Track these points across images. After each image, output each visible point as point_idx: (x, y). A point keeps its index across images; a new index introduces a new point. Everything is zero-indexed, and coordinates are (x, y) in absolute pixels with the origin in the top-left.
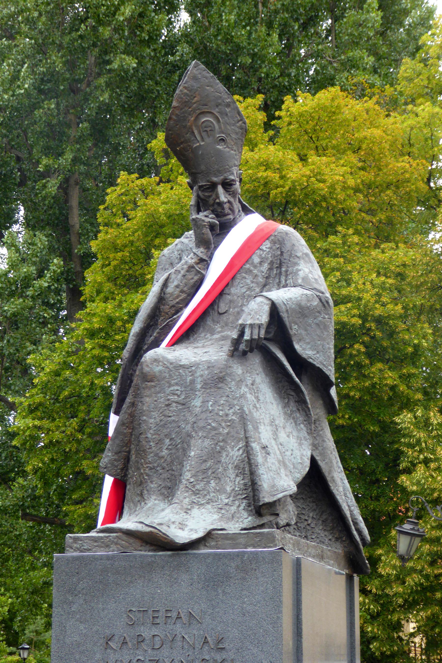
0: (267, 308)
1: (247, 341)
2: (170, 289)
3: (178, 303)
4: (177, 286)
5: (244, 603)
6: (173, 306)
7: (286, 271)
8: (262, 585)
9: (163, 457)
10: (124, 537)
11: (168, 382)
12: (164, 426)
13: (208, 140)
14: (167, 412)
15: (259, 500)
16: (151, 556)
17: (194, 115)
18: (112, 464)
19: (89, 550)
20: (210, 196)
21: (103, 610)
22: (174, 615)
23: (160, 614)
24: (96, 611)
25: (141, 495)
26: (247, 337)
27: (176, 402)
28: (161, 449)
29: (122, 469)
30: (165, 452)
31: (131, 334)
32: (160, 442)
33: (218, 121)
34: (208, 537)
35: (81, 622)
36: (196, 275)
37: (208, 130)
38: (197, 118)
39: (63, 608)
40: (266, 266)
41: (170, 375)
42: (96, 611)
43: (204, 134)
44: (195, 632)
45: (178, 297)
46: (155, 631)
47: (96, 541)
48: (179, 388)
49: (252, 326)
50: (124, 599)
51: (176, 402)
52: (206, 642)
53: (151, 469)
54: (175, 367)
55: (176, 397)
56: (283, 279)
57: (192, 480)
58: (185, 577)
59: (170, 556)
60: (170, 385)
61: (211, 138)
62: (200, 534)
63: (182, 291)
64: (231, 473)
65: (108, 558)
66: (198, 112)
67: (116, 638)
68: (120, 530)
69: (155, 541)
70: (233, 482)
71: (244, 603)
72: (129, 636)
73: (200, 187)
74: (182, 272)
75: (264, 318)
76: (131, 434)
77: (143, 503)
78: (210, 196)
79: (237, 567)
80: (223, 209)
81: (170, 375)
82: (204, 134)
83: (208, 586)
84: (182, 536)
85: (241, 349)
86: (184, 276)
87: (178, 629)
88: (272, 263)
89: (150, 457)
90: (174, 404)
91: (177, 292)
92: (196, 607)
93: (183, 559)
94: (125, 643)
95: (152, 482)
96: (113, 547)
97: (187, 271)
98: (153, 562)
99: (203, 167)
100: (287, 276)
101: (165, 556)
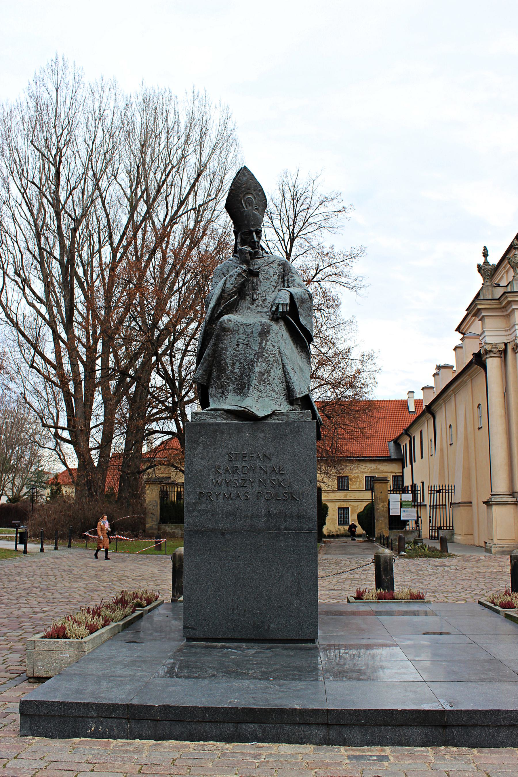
0: (288, 296)
1: (280, 312)
2: (228, 285)
3: (232, 293)
4: (232, 284)
5: (295, 449)
6: (230, 294)
7: (288, 280)
8: (305, 440)
9: (236, 373)
10: (225, 414)
11: (238, 333)
12: (236, 356)
13: (250, 208)
14: (237, 349)
15: (293, 396)
16: (242, 424)
17: (243, 194)
18: (202, 377)
19: (204, 420)
20: (248, 238)
21: (214, 452)
22: (255, 455)
23: (247, 455)
24: (210, 453)
25: (223, 393)
26: (281, 310)
27: (243, 344)
28: (234, 369)
29: (207, 380)
30: (237, 370)
31: (209, 307)
32: (233, 365)
33: (255, 198)
34: (273, 413)
35: (201, 459)
36: (242, 278)
37: (249, 203)
38: (244, 196)
39: (191, 451)
40: (276, 277)
41: (238, 329)
42: (210, 453)
43: (247, 204)
44: (267, 465)
45: (232, 289)
46: (244, 464)
47: (209, 415)
48: (244, 336)
49: (283, 304)
50: (227, 447)
51: (243, 344)
52: (274, 470)
53: (228, 379)
54: (241, 325)
55: (242, 340)
56: (286, 284)
57: (257, 384)
58: (262, 435)
59: (252, 424)
60: (239, 334)
61: (251, 207)
62: (270, 413)
63: (234, 287)
64: (277, 381)
65: (217, 424)
66: (245, 192)
67: (222, 467)
68: (223, 410)
69: (245, 416)
70: (279, 387)
71: (295, 449)
72: (230, 467)
73: (243, 233)
74: (234, 277)
75: (288, 301)
76: (213, 361)
77: (224, 398)
78: (248, 238)
79: (291, 430)
80: (255, 245)
81: (238, 329)
82: (247, 204)
83: (274, 440)
84: (261, 414)
85: (276, 316)
86: (235, 279)
87: (258, 463)
88: (279, 276)
89: (228, 372)
90: (241, 344)
91: (232, 287)
92: (267, 452)
93: (260, 425)
94: (227, 470)
95: (229, 386)
96: (219, 418)
97: (238, 276)
98: (242, 427)
99: (246, 222)
100: (288, 282)
101: (250, 424)
